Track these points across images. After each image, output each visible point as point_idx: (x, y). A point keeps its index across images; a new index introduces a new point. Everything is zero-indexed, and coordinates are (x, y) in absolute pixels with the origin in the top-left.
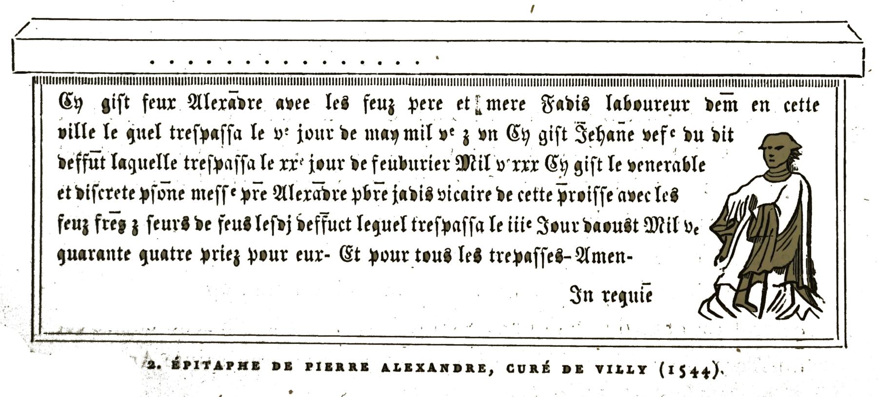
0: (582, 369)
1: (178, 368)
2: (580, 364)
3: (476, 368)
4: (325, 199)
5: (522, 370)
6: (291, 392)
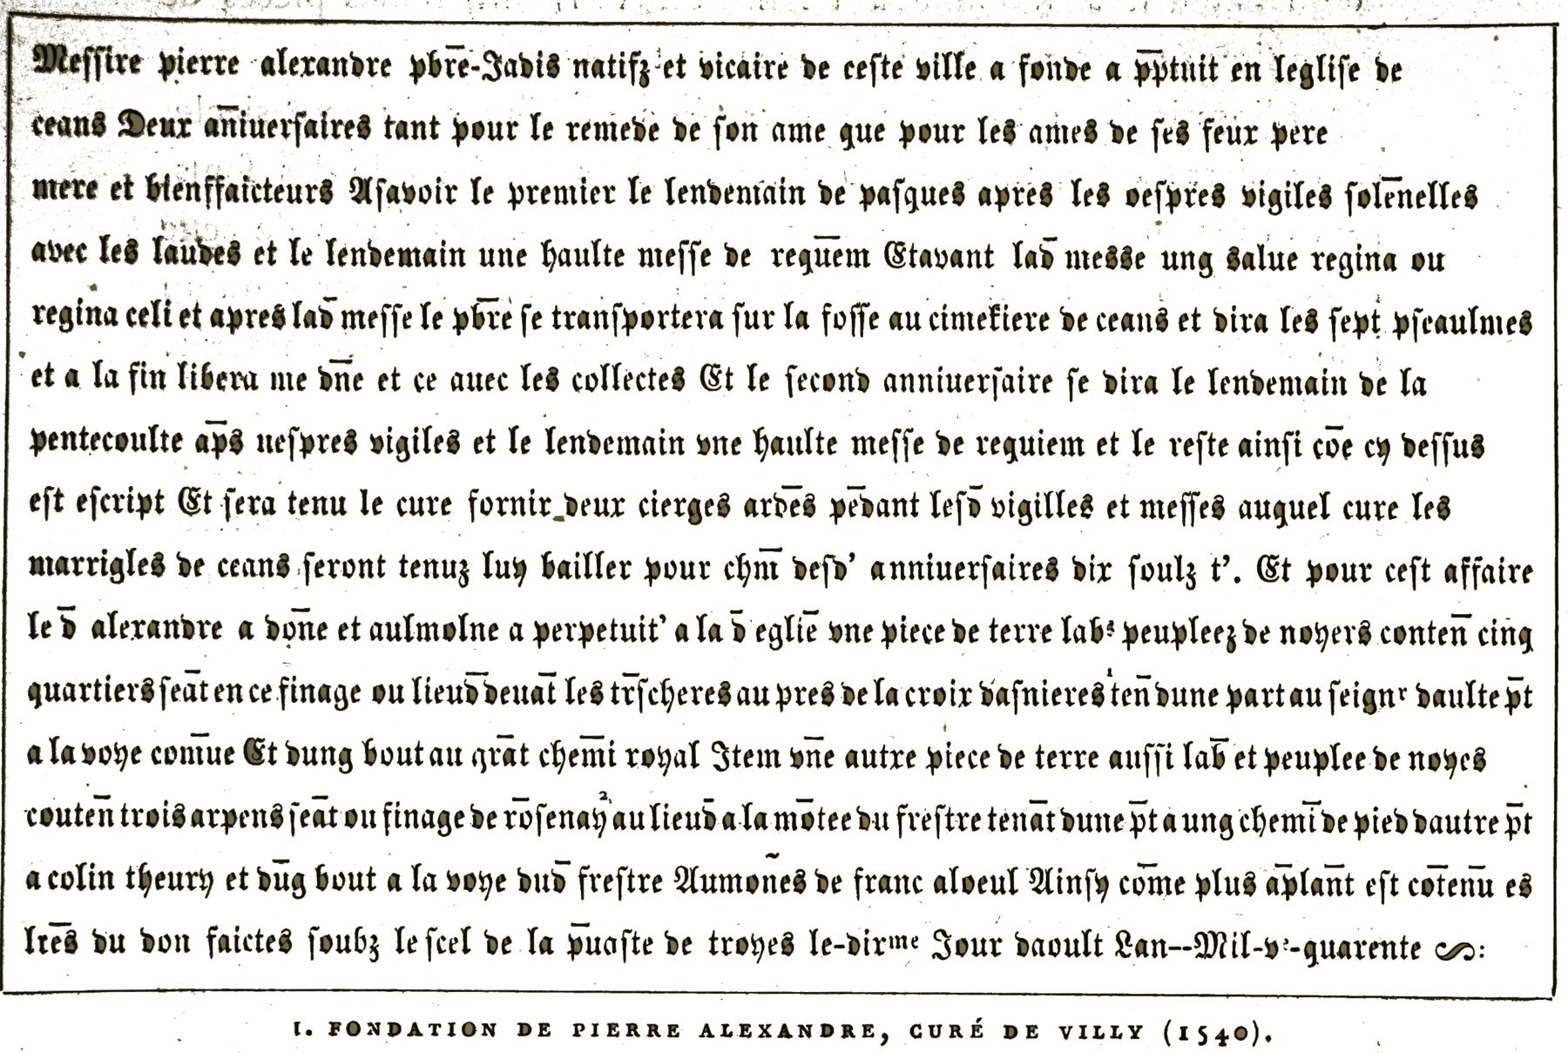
3: (858, 1031)
4: (185, 636)
5: (936, 1033)
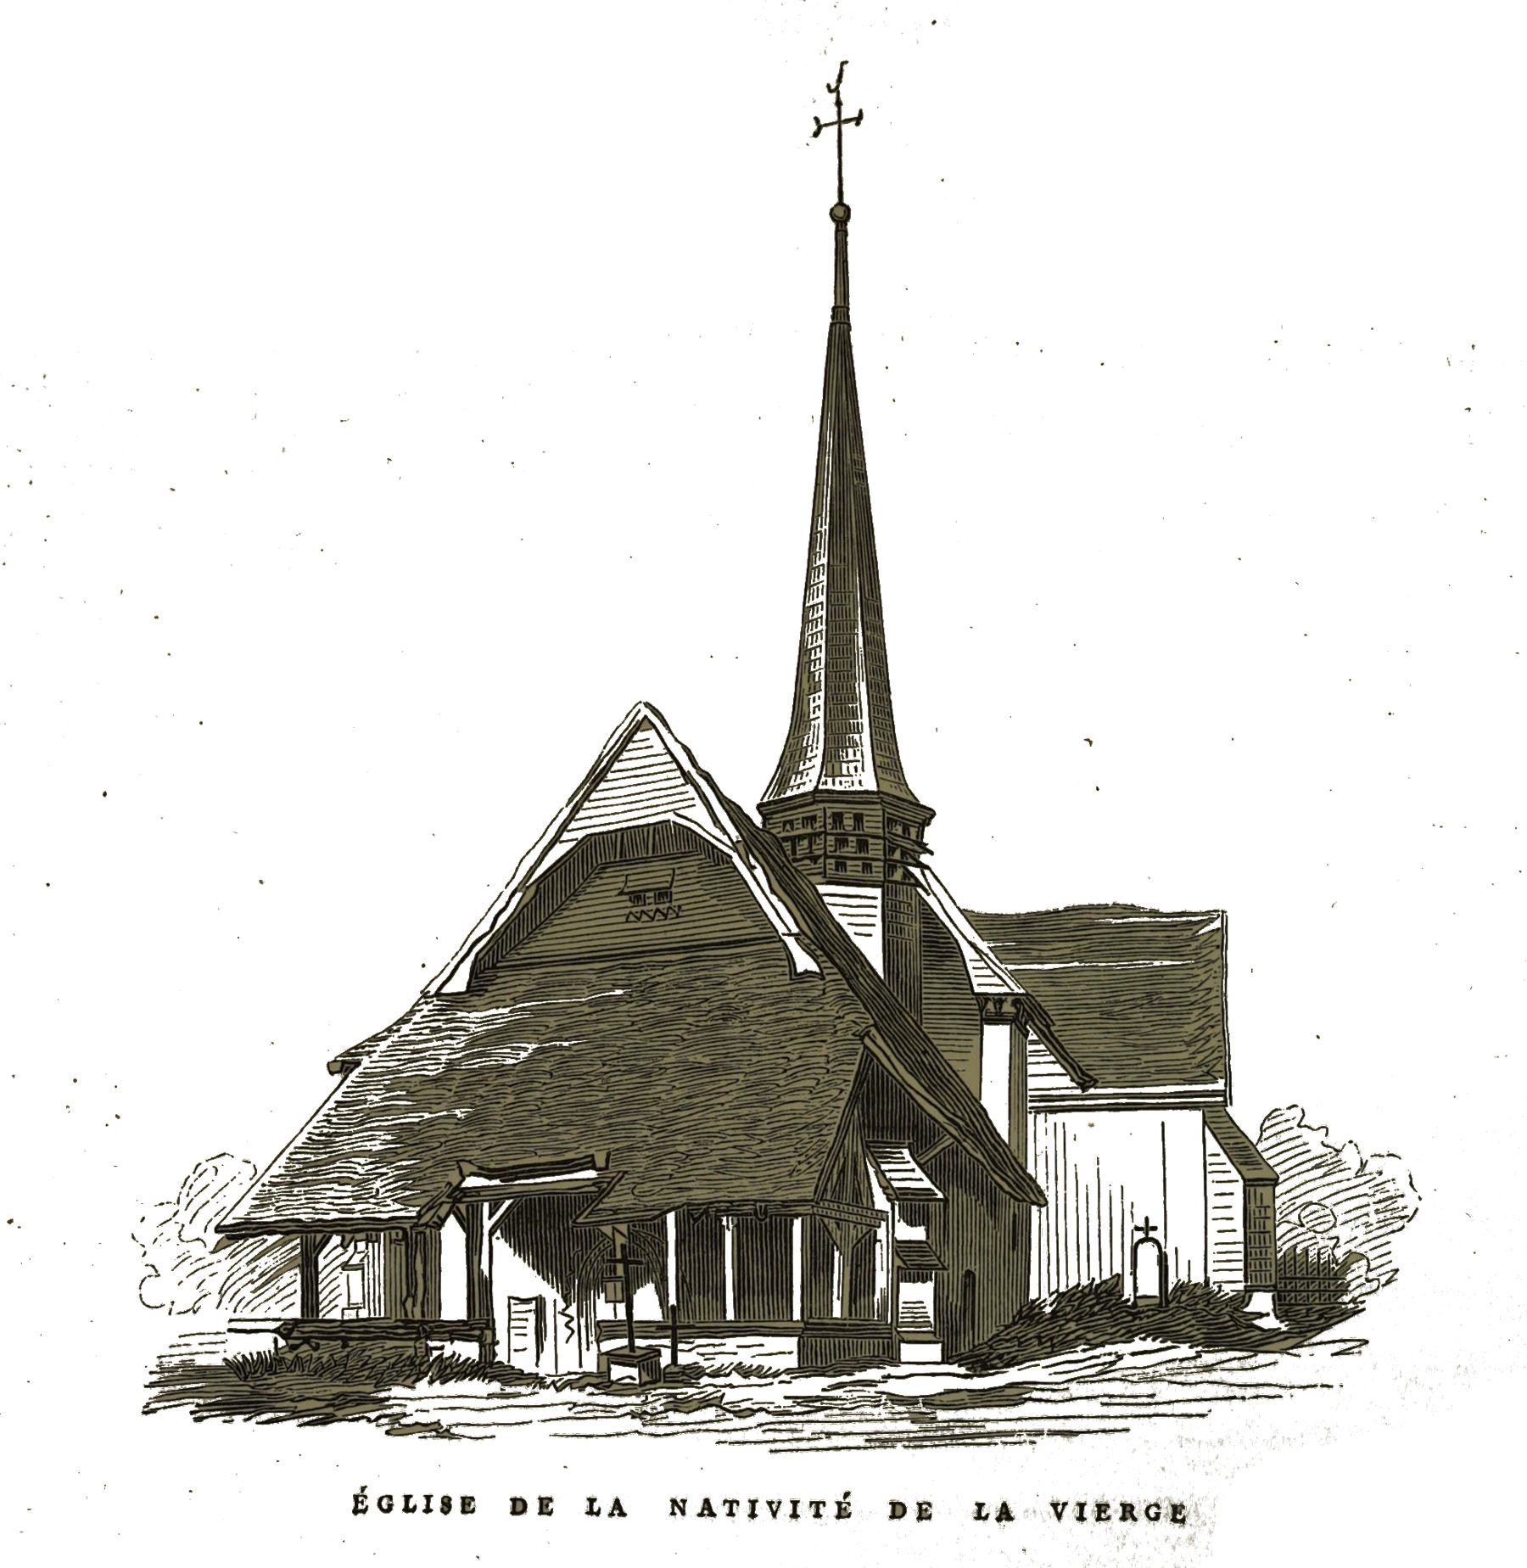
2: (471, 1495)
6: (201, 723)
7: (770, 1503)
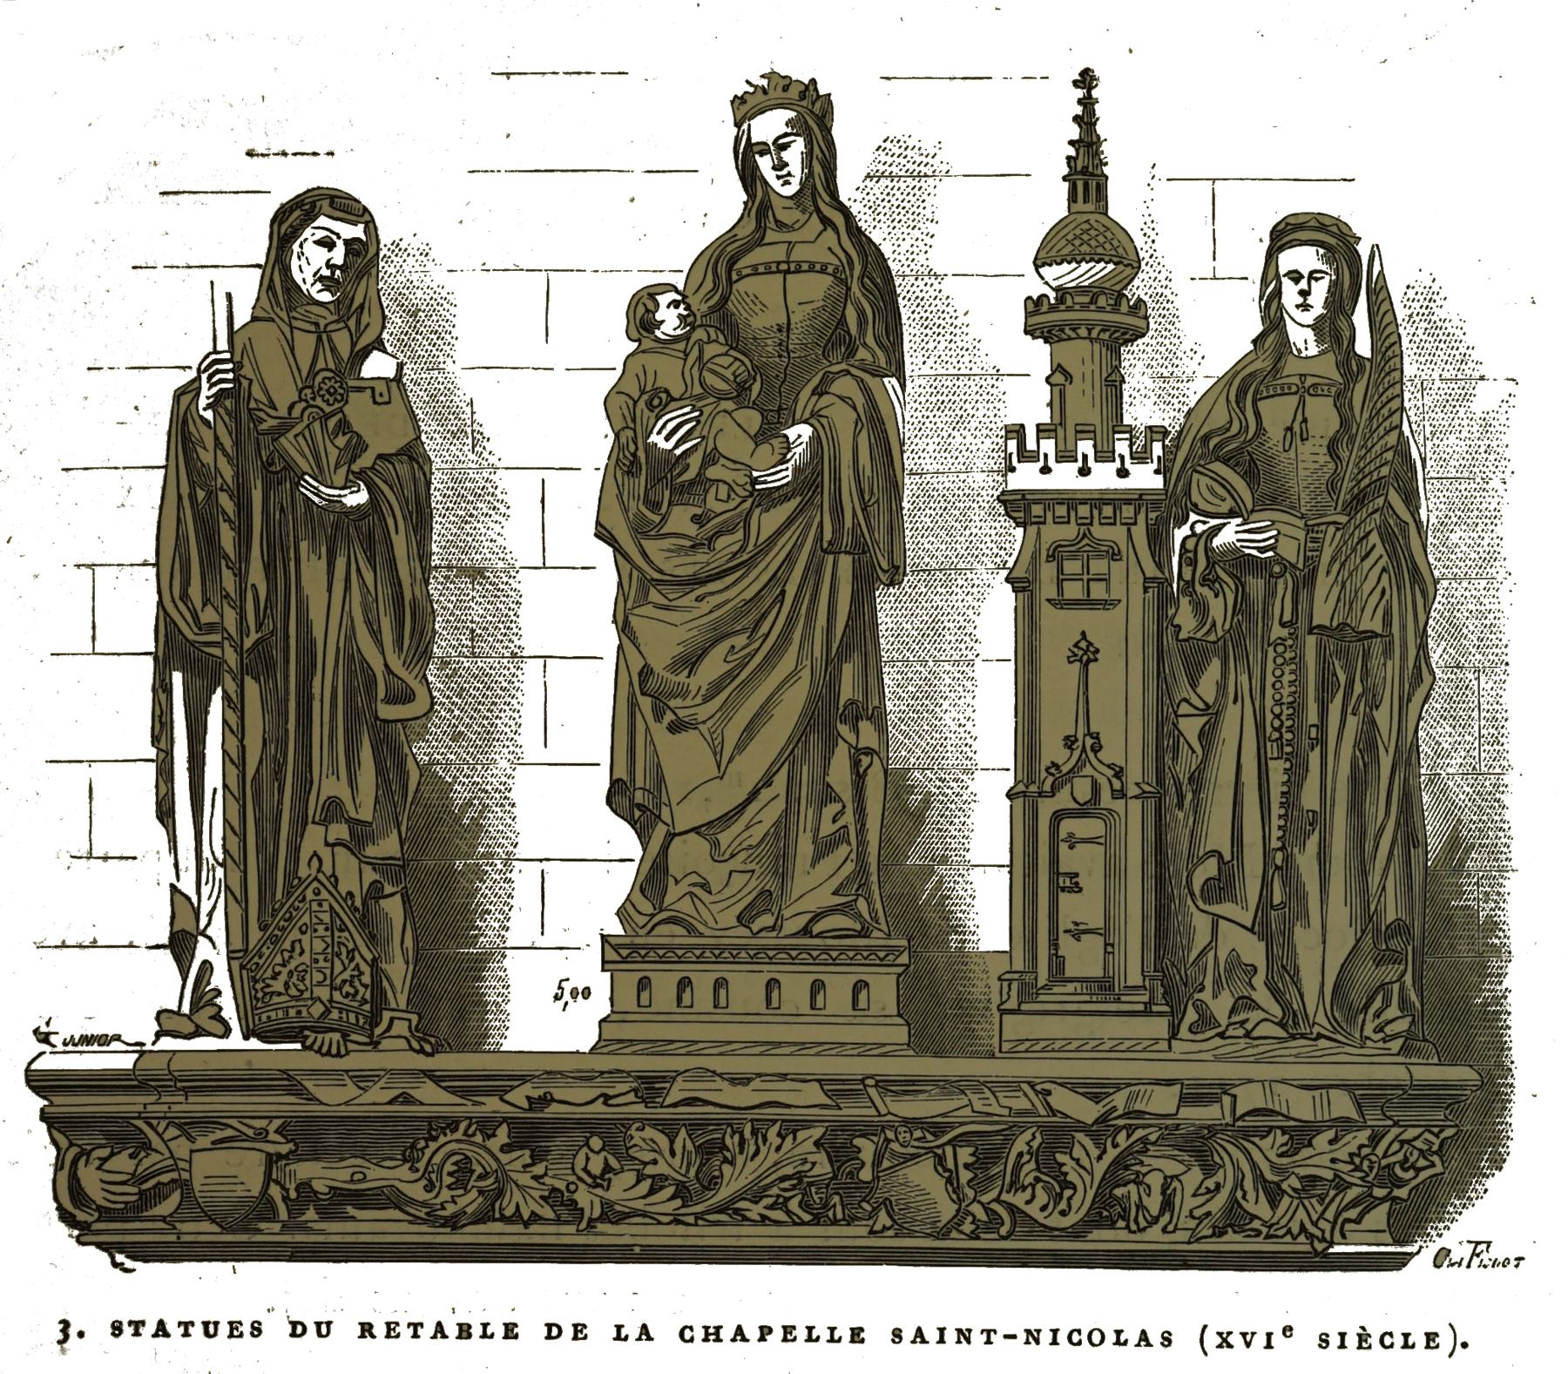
0: (516, 1330)
1: (469, 1336)
7: (1244, 1335)
